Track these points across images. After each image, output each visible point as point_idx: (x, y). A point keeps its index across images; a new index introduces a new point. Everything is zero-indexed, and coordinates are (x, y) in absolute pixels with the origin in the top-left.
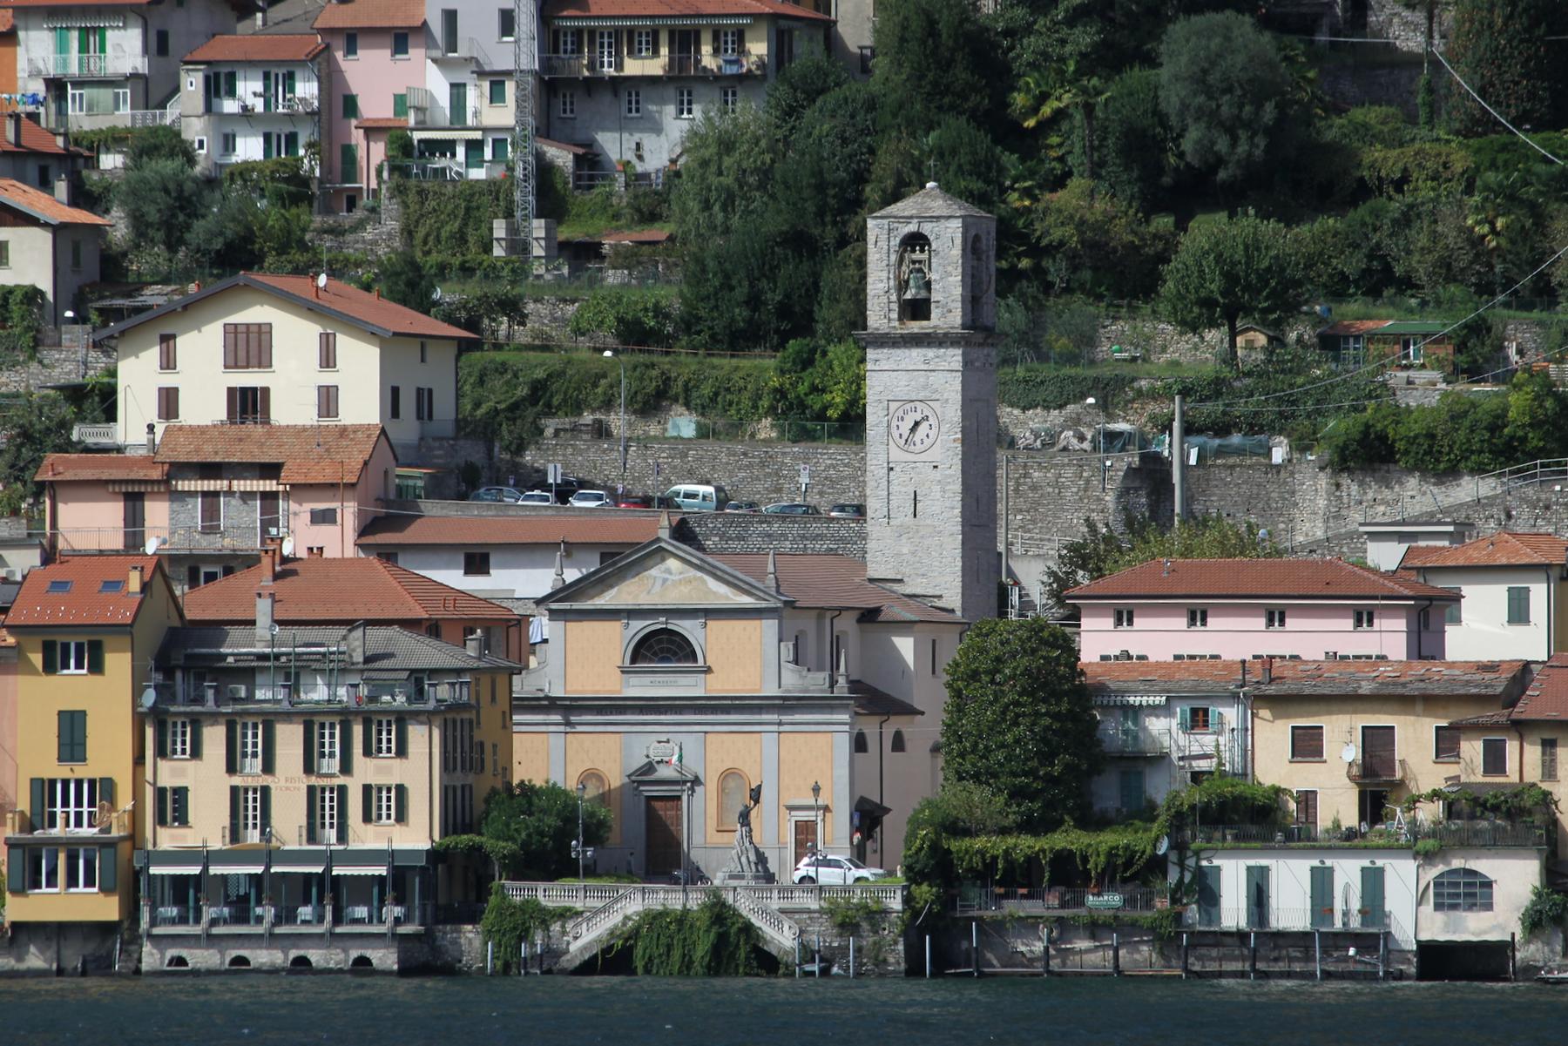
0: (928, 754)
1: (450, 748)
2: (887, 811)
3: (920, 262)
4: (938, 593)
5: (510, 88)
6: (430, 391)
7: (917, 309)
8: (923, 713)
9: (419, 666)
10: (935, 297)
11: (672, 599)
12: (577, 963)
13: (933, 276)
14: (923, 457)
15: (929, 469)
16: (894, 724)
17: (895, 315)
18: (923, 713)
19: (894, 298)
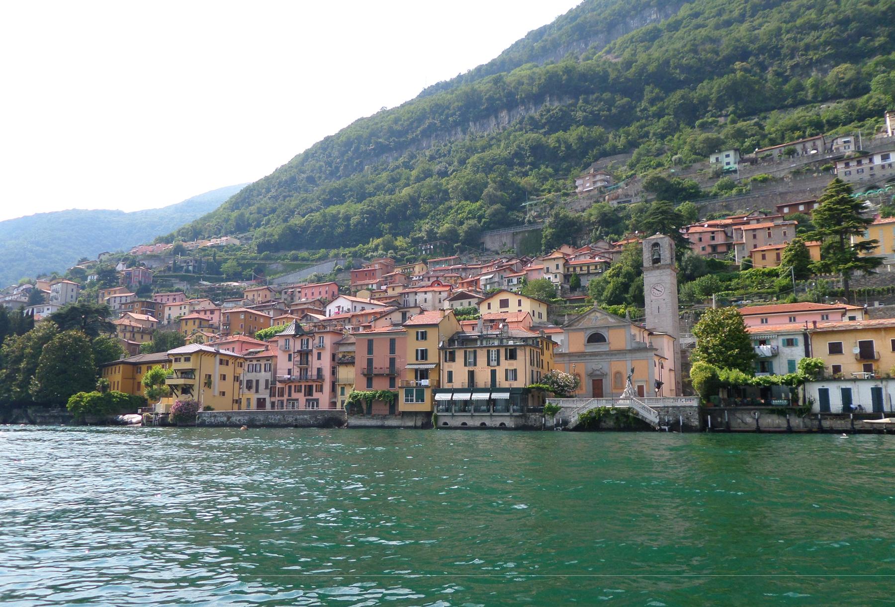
7: (656, 261)
11: (600, 323)
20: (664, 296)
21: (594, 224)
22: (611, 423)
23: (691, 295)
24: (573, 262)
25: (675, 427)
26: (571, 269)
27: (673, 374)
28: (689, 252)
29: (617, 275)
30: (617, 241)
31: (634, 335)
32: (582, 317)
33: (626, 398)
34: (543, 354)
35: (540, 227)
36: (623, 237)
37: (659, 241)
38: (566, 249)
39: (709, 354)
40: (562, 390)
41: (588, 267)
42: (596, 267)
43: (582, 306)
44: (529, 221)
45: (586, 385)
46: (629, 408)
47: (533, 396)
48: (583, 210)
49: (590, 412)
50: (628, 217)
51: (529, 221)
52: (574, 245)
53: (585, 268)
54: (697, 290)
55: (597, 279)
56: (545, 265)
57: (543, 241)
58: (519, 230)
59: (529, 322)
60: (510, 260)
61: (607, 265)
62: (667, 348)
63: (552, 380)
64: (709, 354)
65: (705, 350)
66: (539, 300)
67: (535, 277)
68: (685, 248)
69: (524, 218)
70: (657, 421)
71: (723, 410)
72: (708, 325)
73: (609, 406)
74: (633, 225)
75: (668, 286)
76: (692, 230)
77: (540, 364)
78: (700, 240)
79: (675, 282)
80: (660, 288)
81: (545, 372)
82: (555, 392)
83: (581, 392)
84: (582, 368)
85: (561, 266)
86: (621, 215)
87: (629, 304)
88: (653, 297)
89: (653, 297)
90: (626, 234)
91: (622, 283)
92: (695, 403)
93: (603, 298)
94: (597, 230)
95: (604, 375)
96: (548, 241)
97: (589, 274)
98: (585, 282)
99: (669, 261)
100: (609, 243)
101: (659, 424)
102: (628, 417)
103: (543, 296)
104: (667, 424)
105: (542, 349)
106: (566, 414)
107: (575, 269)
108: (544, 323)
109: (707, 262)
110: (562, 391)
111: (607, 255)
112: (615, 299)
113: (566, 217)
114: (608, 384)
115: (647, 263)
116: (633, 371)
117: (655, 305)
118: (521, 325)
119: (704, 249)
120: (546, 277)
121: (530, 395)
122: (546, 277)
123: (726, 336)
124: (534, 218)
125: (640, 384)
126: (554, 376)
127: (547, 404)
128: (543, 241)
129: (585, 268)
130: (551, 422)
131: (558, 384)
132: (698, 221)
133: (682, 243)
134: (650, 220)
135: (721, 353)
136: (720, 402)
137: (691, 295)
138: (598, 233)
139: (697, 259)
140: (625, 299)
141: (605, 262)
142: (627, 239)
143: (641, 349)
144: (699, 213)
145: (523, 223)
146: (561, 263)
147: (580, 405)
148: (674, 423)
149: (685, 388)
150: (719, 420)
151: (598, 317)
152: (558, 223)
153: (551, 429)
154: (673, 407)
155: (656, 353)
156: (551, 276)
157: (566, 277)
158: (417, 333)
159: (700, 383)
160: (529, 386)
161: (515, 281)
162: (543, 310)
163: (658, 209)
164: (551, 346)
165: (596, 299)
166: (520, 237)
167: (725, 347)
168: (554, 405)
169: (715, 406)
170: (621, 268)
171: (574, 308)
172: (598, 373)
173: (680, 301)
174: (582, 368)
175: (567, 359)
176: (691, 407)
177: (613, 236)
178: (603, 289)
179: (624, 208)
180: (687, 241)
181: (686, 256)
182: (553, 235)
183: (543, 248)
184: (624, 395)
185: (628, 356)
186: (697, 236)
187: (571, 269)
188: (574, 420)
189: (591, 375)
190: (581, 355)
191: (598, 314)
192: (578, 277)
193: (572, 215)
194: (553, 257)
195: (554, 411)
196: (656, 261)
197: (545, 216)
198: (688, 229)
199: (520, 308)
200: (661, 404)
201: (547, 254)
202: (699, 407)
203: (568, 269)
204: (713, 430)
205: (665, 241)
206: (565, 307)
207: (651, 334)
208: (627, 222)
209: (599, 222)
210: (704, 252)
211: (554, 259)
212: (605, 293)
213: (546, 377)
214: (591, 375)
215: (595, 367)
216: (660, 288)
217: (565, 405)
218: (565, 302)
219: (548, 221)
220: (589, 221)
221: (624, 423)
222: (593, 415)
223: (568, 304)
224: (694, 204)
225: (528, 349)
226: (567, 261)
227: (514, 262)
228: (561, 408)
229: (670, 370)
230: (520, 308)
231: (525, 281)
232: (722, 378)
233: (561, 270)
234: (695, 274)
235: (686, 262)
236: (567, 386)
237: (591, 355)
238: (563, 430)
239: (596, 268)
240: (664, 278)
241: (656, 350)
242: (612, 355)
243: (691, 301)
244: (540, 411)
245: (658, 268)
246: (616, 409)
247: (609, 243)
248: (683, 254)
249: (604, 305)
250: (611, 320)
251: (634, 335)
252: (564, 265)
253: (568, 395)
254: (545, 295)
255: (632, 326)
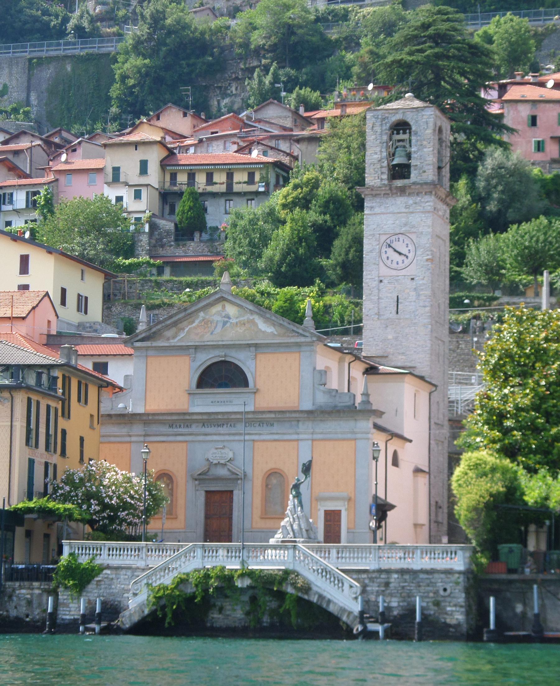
0: (411, 474)
1: (33, 426)
2: (392, 507)
3: (402, 141)
4: (414, 365)
5: (144, 193)
6: (86, 298)
7: (400, 172)
8: (411, 441)
9: (9, 362)
10: (413, 162)
11: (232, 335)
12: (136, 618)
13: (413, 149)
14: (403, 272)
15: (409, 282)
16: (394, 445)
17: (385, 177)
18: (411, 441)
19: (385, 164)
20: (412, 270)
21: (258, 52)
22: (236, 613)
23: (493, 271)
24: (183, 158)
25: (403, 627)
26: (182, 178)
27: (423, 480)
28: (499, 153)
29: (304, 203)
30: (316, 107)
31: (324, 373)
32: (188, 313)
33: (282, 546)
34: (66, 414)
35: (109, 48)
36: (334, 98)
37: (410, 118)
38: (176, 120)
39: (506, 432)
40: (112, 519)
41: (230, 176)
42: (251, 176)
43: (204, 284)
44: (79, 30)
45: (189, 504)
46: (287, 573)
47: (28, 534)
48: (234, 12)
49: (182, 582)
50: (352, 43)
51: (79, 29)
52: (201, 110)
53: (220, 178)
54: (508, 257)
55: (257, 209)
56: (109, 160)
57: (115, 91)
58: (48, 50)
59: (45, 321)
60: (14, 137)
61: (282, 172)
62: (410, 409)
63: (85, 490)
64: (506, 432)
65: (496, 419)
66: (85, 261)
67: (79, 193)
68: (489, 141)
69: (66, 20)
70: (356, 607)
71: (529, 583)
72: (508, 354)
73: (233, 565)
74: (364, 66)
75: (425, 241)
76: (514, 93)
77: (57, 443)
78: (534, 121)
79: (447, 229)
80: (404, 244)
81: (70, 465)
82: (91, 523)
83: (169, 525)
84: (175, 456)
85: (154, 168)
86: (333, 34)
87: (331, 285)
88: (384, 271)
89: (384, 271)
90: (343, 89)
91: (317, 228)
92: (458, 562)
93: (261, 264)
94: (266, 69)
95: (236, 478)
96: (130, 90)
97: (229, 193)
98: (217, 216)
99: (430, 175)
100: (296, 112)
101: (362, 617)
102: (281, 595)
103: (97, 247)
104: (383, 618)
105: (65, 401)
106: (117, 587)
107: (191, 176)
108: (92, 327)
109: (543, 183)
110: (112, 521)
111: (284, 146)
112: (295, 270)
113: (183, 25)
114: (248, 504)
115: (375, 176)
116: (307, 469)
117: (388, 295)
118: (22, 328)
119: (540, 147)
120: (111, 193)
121: (20, 531)
122: (111, 193)
123: (549, 385)
124: (92, 21)
125: (332, 506)
126: (91, 476)
127: (65, 557)
128: (115, 91)
129: (220, 178)
130: (74, 608)
131: (101, 503)
132: (535, 68)
133: (483, 126)
134: (403, 56)
135: (536, 430)
136: (523, 561)
137: (493, 271)
138: (268, 80)
139: (519, 174)
140: (320, 272)
141: (278, 165)
142: (342, 105)
143: (343, 410)
144: (539, 47)
145: (61, 33)
146: (154, 157)
147: (156, 561)
148: (402, 617)
149: (445, 525)
150: (519, 608)
151: (228, 320)
152: (161, 43)
153: (71, 627)
154: (402, 572)
155: (380, 422)
156: (123, 192)
157: (167, 198)
158: (29, 400)
159: (475, 509)
160: (18, 503)
161: (20, 199)
162: (93, 287)
163: (425, 26)
164: (93, 391)
165: (245, 265)
166: (47, 73)
167: (547, 415)
168: (84, 560)
169: (511, 571)
170: (316, 184)
171: (181, 287)
172: (222, 472)
173: (456, 280)
174: (175, 456)
175: (138, 429)
176: (449, 572)
177: (306, 92)
178: (265, 240)
179: (345, 17)
180: (497, 123)
181: (489, 163)
182: (144, 75)
183: (114, 110)
184: (279, 536)
185: (306, 427)
186: (525, 111)
187: (182, 178)
188: (136, 603)
189: (201, 478)
190: (178, 421)
191: (231, 310)
192: (199, 200)
193: (200, 22)
194: (134, 137)
195: (82, 577)
196: (400, 172)
197: (125, 20)
198: (503, 89)
199: (24, 280)
200: (369, 563)
201: (123, 126)
202: (467, 573)
203: (174, 176)
204: (503, 636)
205: (426, 119)
206: (158, 285)
207: (371, 370)
208: (349, 56)
209: (274, 48)
210: (539, 157)
211: (136, 145)
212: (268, 252)
213: (70, 480)
214: (201, 478)
215: (214, 455)
216: (404, 244)
217: (115, 561)
218: (160, 270)
219: (133, 32)
220: (246, 45)
221: (273, 612)
222: (190, 590)
223: (167, 276)
224: (525, 23)
225: (20, 399)
226: (171, 153)
227: (24, 144)
228: (102, 568)
229: (418, 471)
230: (24, 280)
231: (49, 204)
232: (531, 497)
233: (154, 177)
234: (511, 214)
235: (488, 179)
236: (125, 506)
237: (204, 423)
238: (105, 631)
239: (251, 180)
240: (415, 219)
241: (380, 414)
242: (261, 422)
243: (494, 285)
244: (46, 576)
245: (402, 191)
246: (251, 574)
247: (296, 112)
248: (481, 156)
249: (265, 285)
250: (265, 328)
251: (324, 373)
252: (163, 165)
253: (131, 531)
254: (105, 248)
255: (319, 347)
